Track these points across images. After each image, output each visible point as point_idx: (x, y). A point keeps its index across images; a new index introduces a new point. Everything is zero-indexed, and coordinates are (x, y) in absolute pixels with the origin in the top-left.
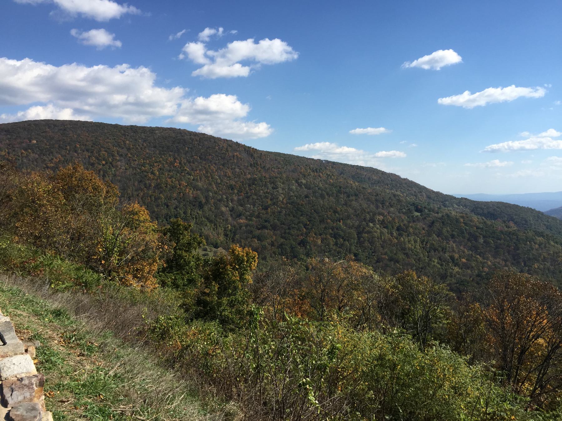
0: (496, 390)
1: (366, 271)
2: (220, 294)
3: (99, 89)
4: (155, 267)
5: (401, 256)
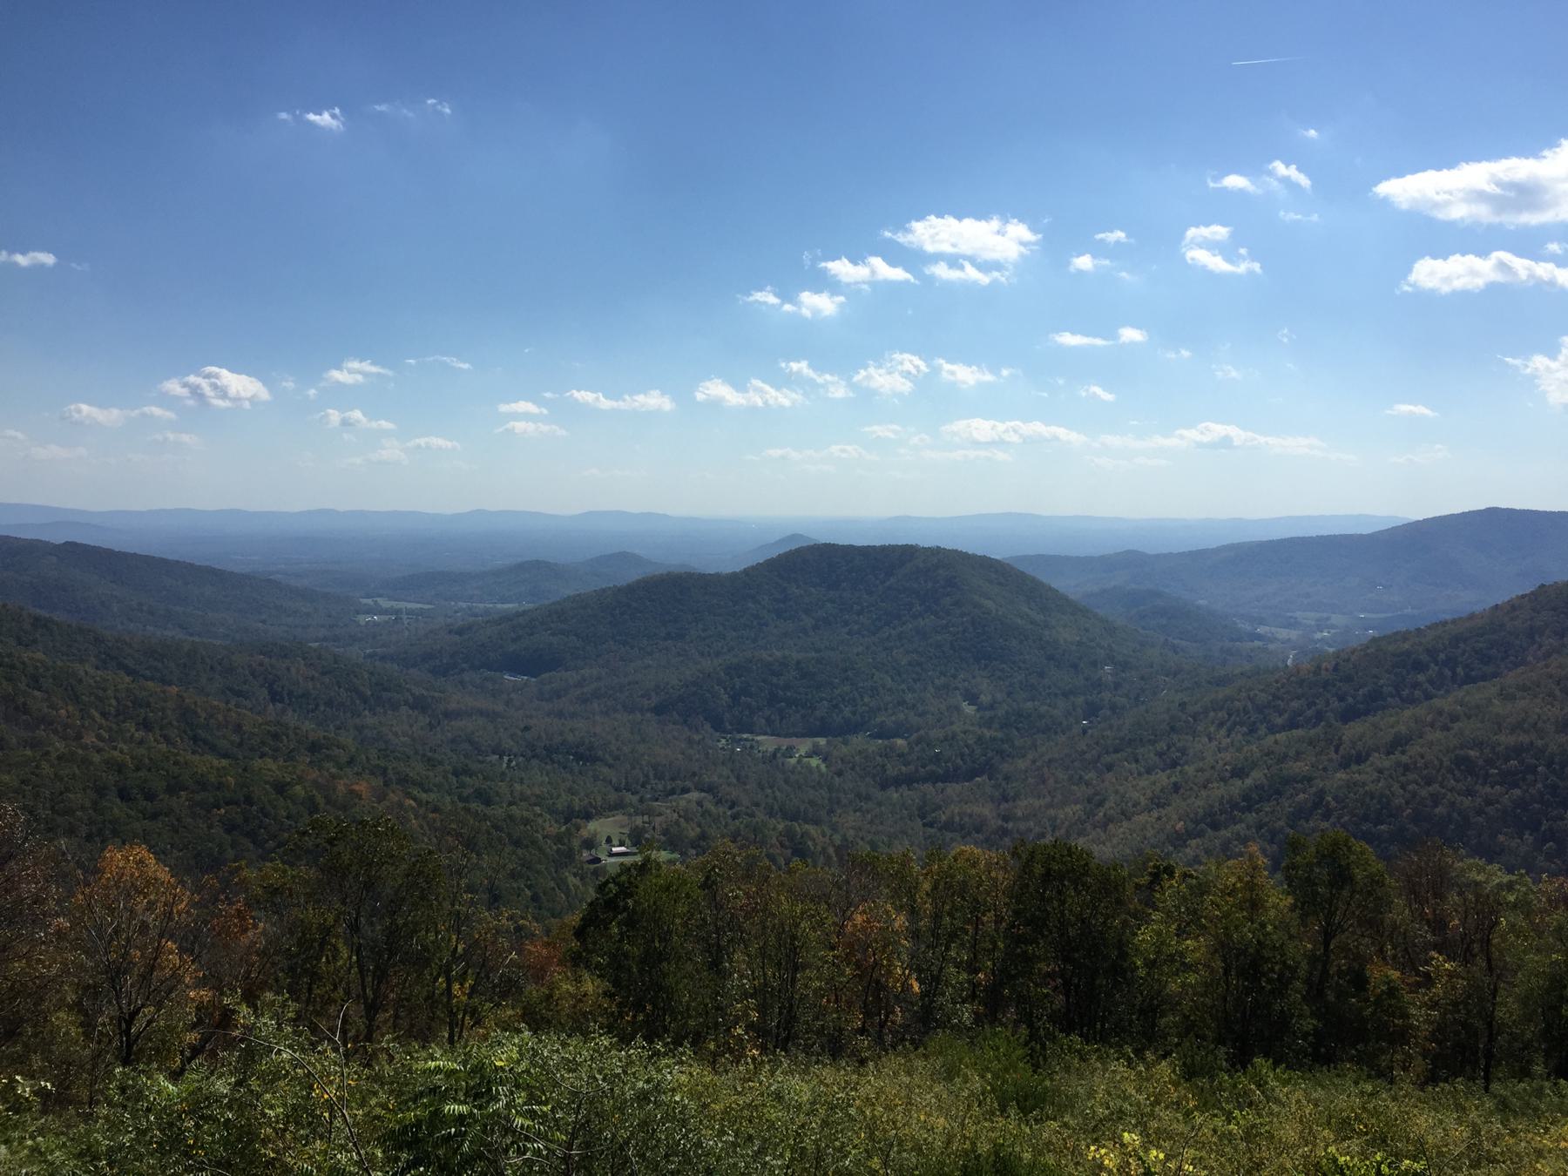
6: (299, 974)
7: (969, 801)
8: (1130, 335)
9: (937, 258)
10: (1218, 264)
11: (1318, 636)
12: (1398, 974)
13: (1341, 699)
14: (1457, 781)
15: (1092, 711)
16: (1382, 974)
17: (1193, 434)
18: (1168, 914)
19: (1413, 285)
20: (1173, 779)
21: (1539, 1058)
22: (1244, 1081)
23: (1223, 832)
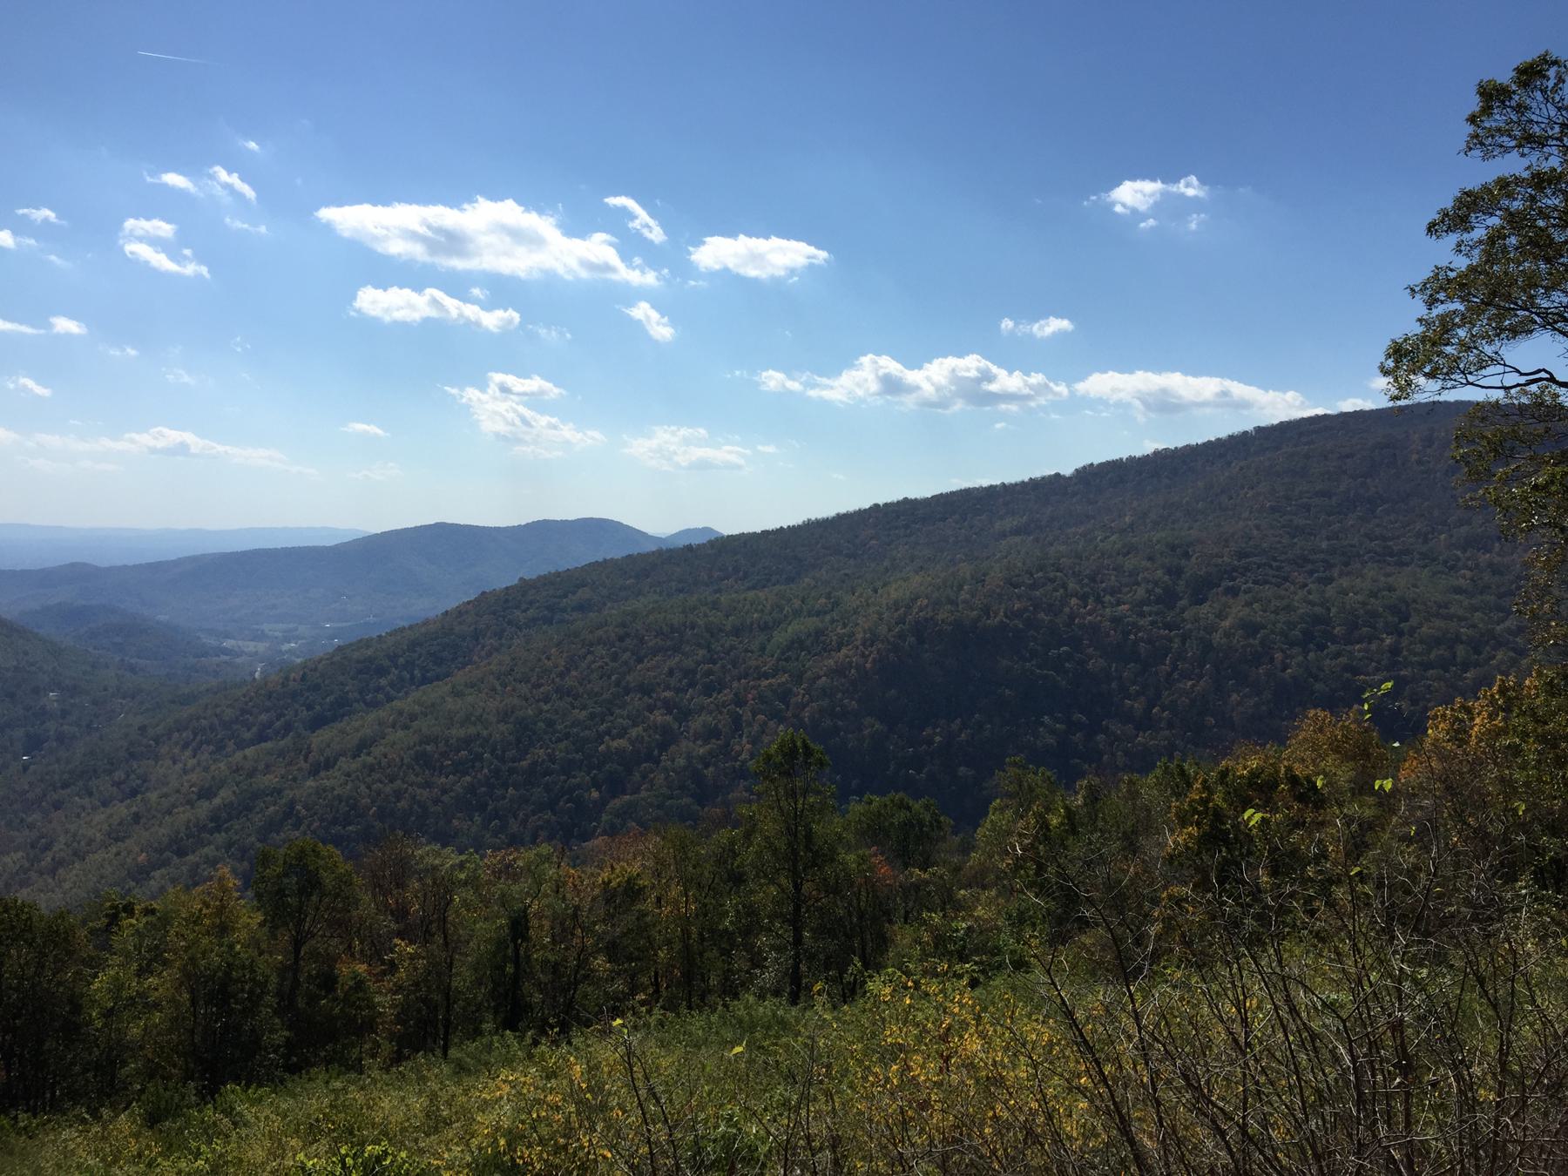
8: (64, 325)
10: (161, 261)
11: (285, 647)
12: (364, 967)
13: (309, 708)
14: (417, 775)
16: (354, 969)
17: (145, 439)
18: (128, 955)
19: (359, 311)
20: (134, 809)
21: (489, 1016)
22: (209, 1113)
23: (191, 858)
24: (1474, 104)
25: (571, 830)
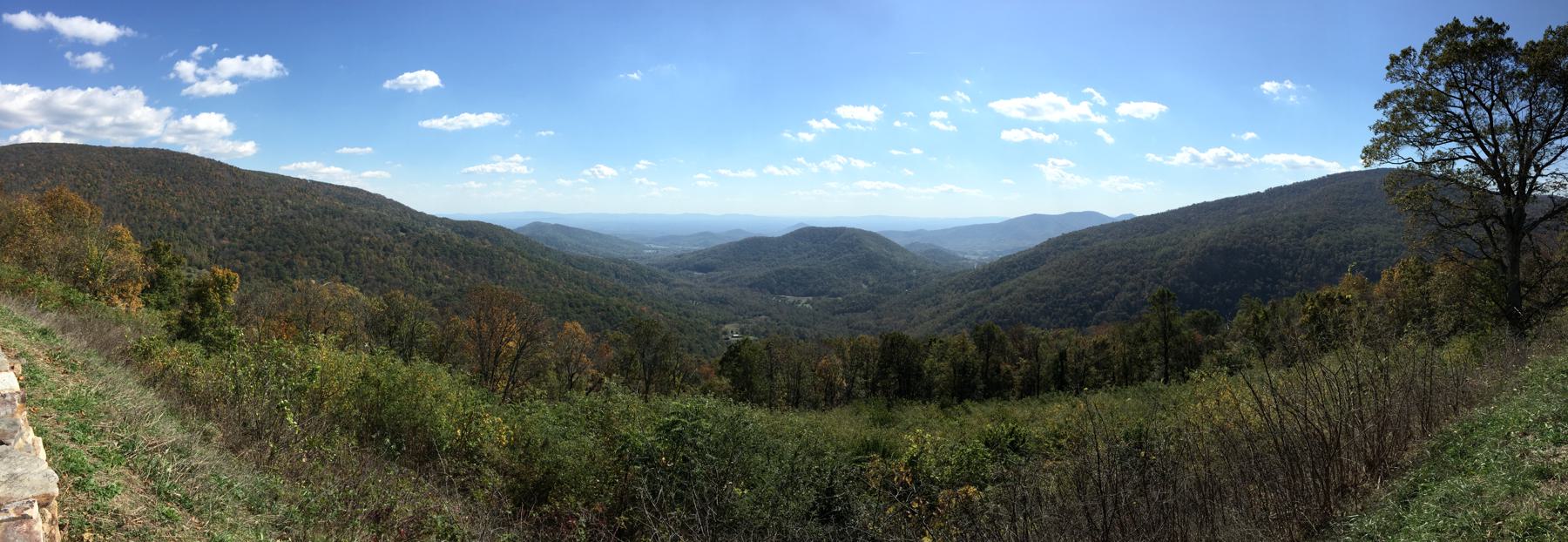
0: (473, 392)
1: (353, 291)
2: (204, 314)
3: (90, 111)
4: (139, 287)
5: (388, 276)
6: (624, 367)
7: (861, 319)
8: (916, 151)
9: (847, 120)
10: (942, 127)
15: (909, 286)
16: (1005, 367)
24: (1388, 62)
25: (1082, 323)
